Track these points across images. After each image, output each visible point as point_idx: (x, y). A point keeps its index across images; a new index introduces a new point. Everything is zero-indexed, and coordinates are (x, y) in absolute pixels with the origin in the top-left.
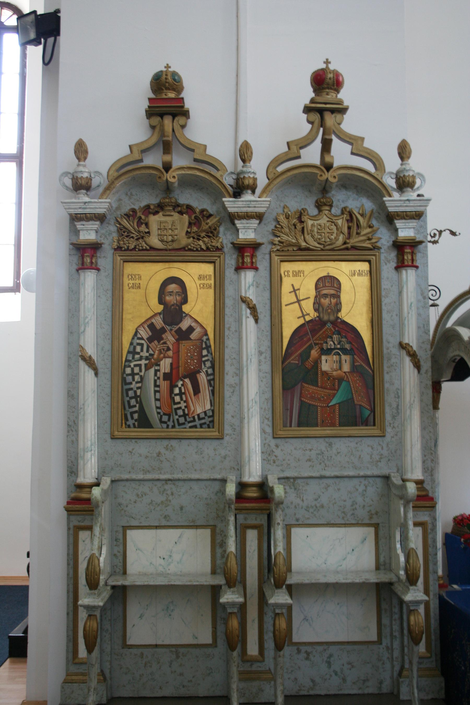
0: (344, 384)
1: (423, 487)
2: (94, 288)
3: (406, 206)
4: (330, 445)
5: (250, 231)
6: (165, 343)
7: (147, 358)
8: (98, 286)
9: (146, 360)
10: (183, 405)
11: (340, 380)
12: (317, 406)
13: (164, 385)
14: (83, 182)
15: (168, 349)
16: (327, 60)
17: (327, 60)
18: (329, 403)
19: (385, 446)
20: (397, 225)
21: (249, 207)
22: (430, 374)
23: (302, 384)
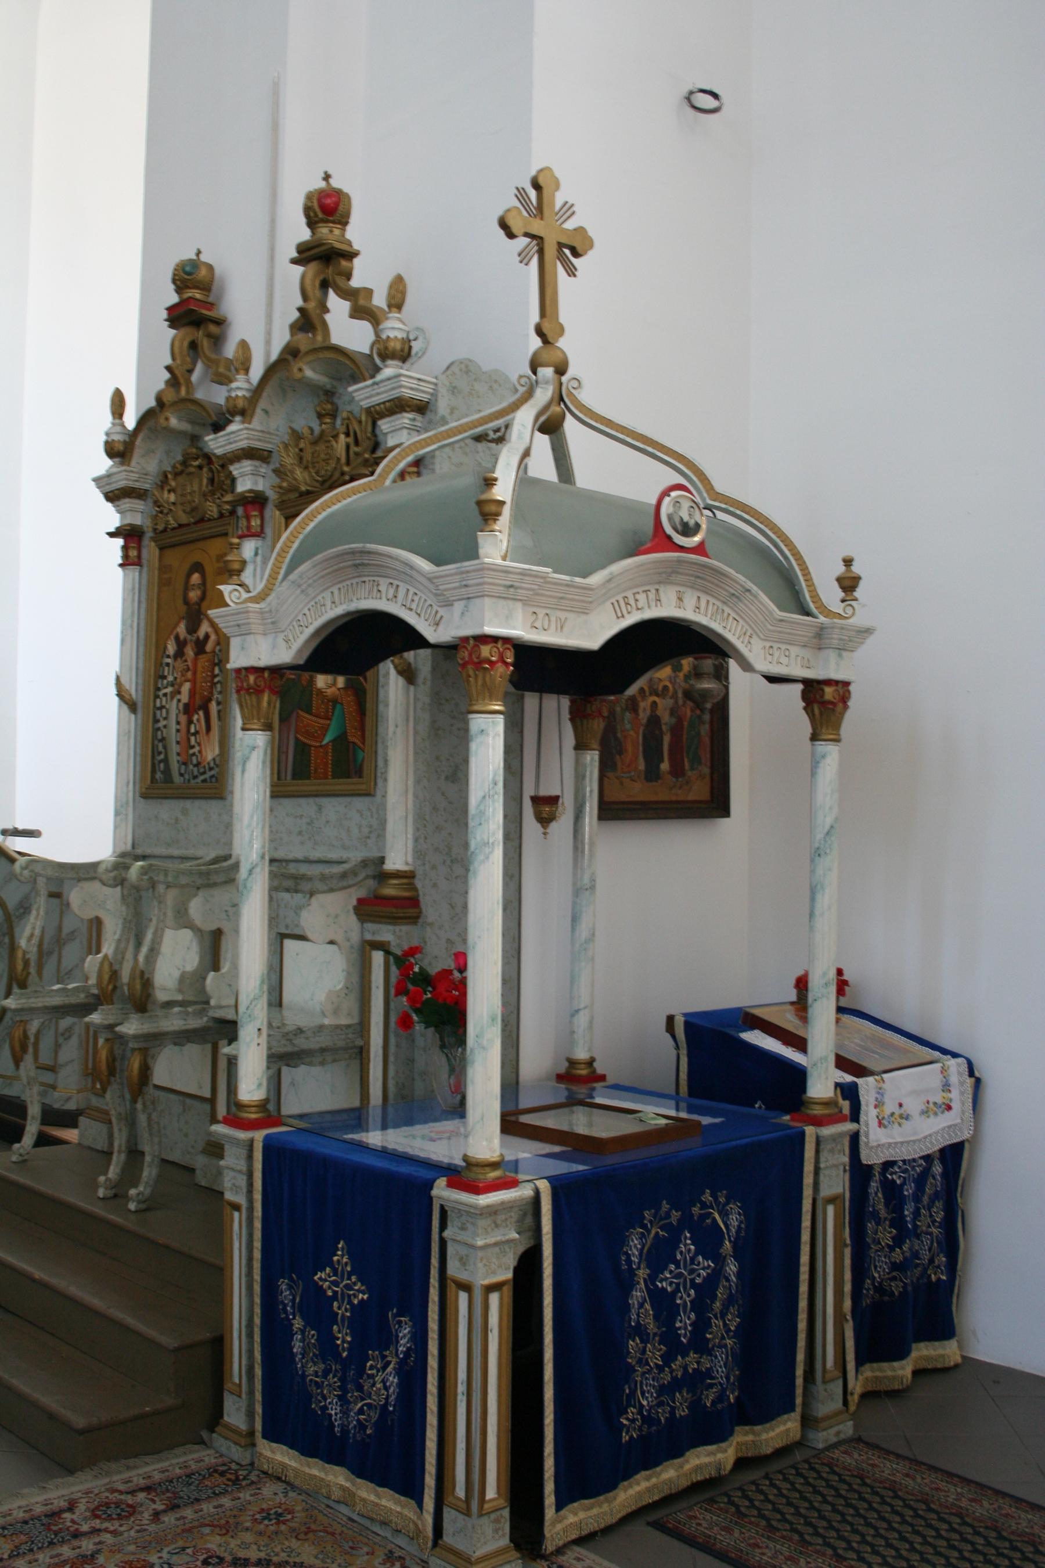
0: (338, 707)
1: (413, 884)
2: (133, 589)
3: (378, 394)
4: (320, 808)
5: (246, 478)
6: (186, 661)
7: (172, 685)
8: (501, 1299)
9: (213, 784)
10: (197, 749)
11: (335, 701)
12: (310, 746)
13: (183, 719)
14: (398, 346)
15: (188, 669)
16: (326, 173)
17: (326, 173)
18: (323, 740)
19: (374, 810)
20: (383, 427)
21: (231, 443)
22: (429, 683)
23: (298, 716)
